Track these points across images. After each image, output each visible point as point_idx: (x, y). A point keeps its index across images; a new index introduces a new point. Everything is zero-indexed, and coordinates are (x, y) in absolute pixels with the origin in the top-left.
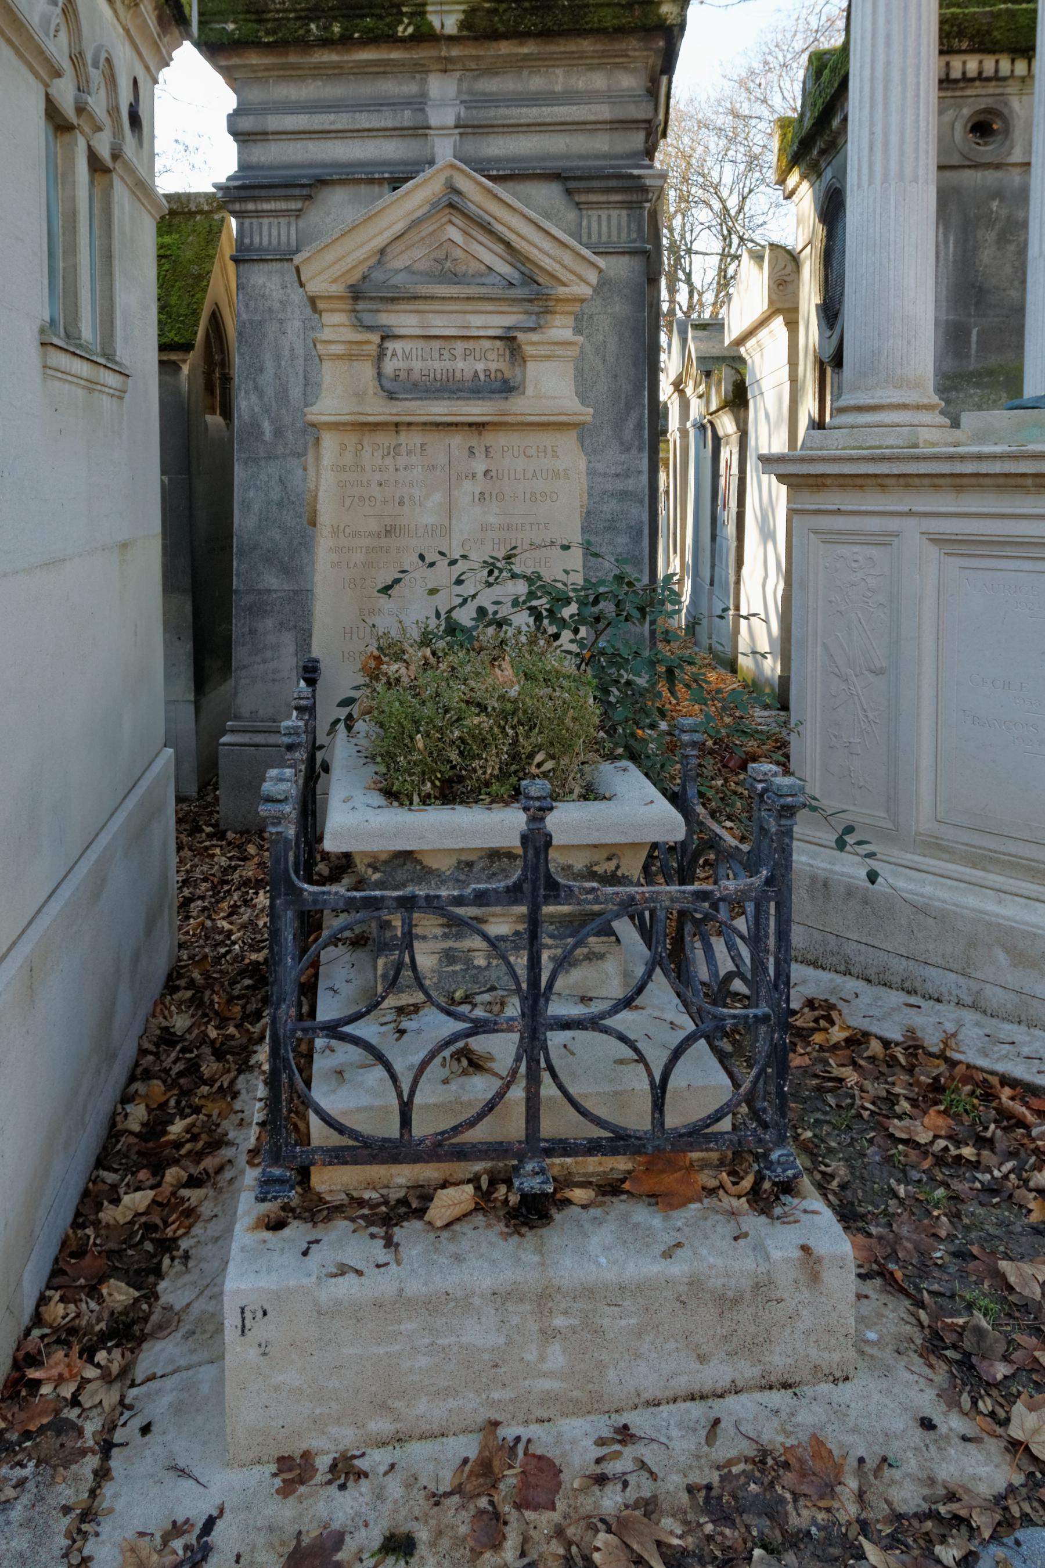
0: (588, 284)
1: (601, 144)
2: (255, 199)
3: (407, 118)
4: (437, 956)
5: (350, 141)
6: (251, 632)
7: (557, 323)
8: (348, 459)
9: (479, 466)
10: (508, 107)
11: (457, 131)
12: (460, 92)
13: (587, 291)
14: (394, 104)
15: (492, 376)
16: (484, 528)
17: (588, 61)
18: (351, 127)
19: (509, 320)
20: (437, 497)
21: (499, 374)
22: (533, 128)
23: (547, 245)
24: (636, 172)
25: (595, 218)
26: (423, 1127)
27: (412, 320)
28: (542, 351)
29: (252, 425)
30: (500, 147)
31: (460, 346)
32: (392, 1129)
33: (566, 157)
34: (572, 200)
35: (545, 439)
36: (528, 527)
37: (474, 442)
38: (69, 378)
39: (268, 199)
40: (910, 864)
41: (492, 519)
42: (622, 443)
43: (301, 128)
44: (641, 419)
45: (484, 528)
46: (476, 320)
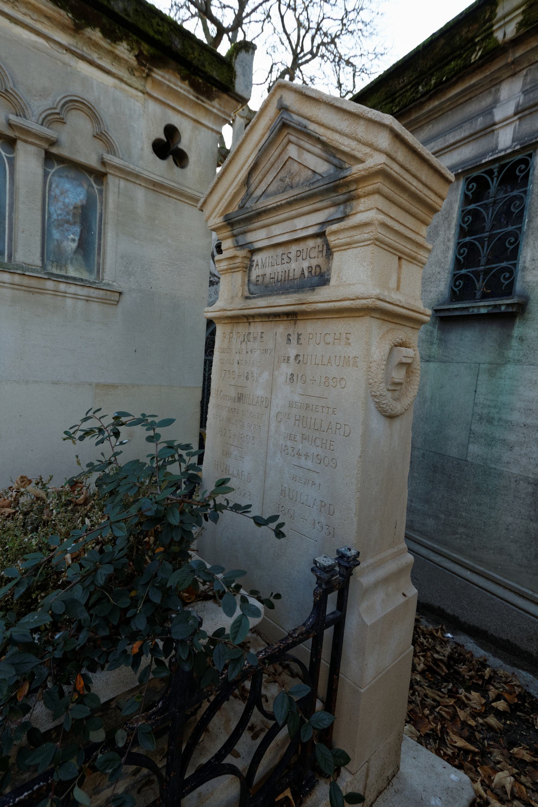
7: (361, 207)
9: (292, 352)
11: (516, 118)
16: (291, 405)
19: (321, 217)
20: (266, 375)
35: (340, 326)
36: (320, 409)
41: (297, 398)
45: (291, 405)
46: (300, 223)
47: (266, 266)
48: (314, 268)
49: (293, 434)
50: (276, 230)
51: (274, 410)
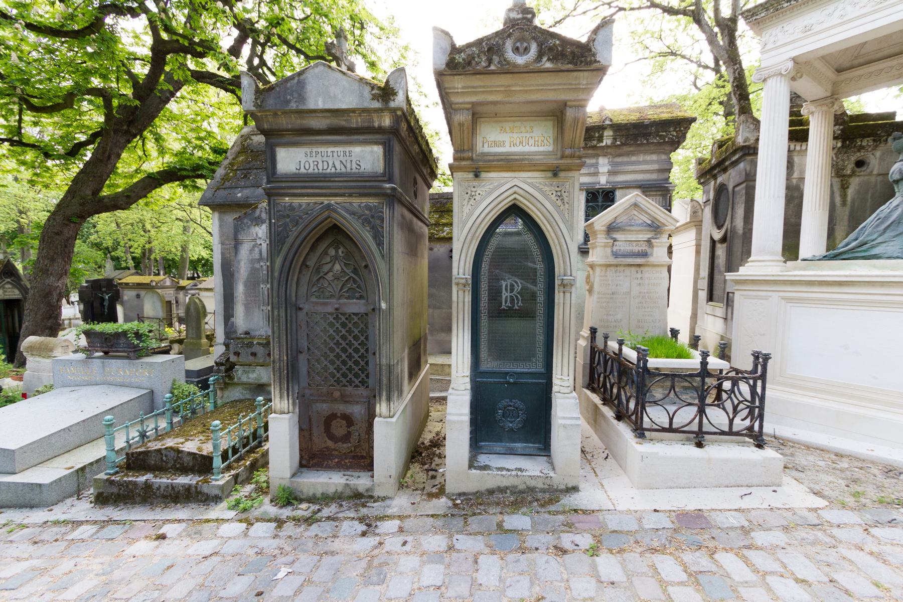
1: (654, 176)
3: (592, 170)
19: (649, 236)
26: (674, 426)
31: (634, 244)
46: (641, 236)
47: (621, 247)
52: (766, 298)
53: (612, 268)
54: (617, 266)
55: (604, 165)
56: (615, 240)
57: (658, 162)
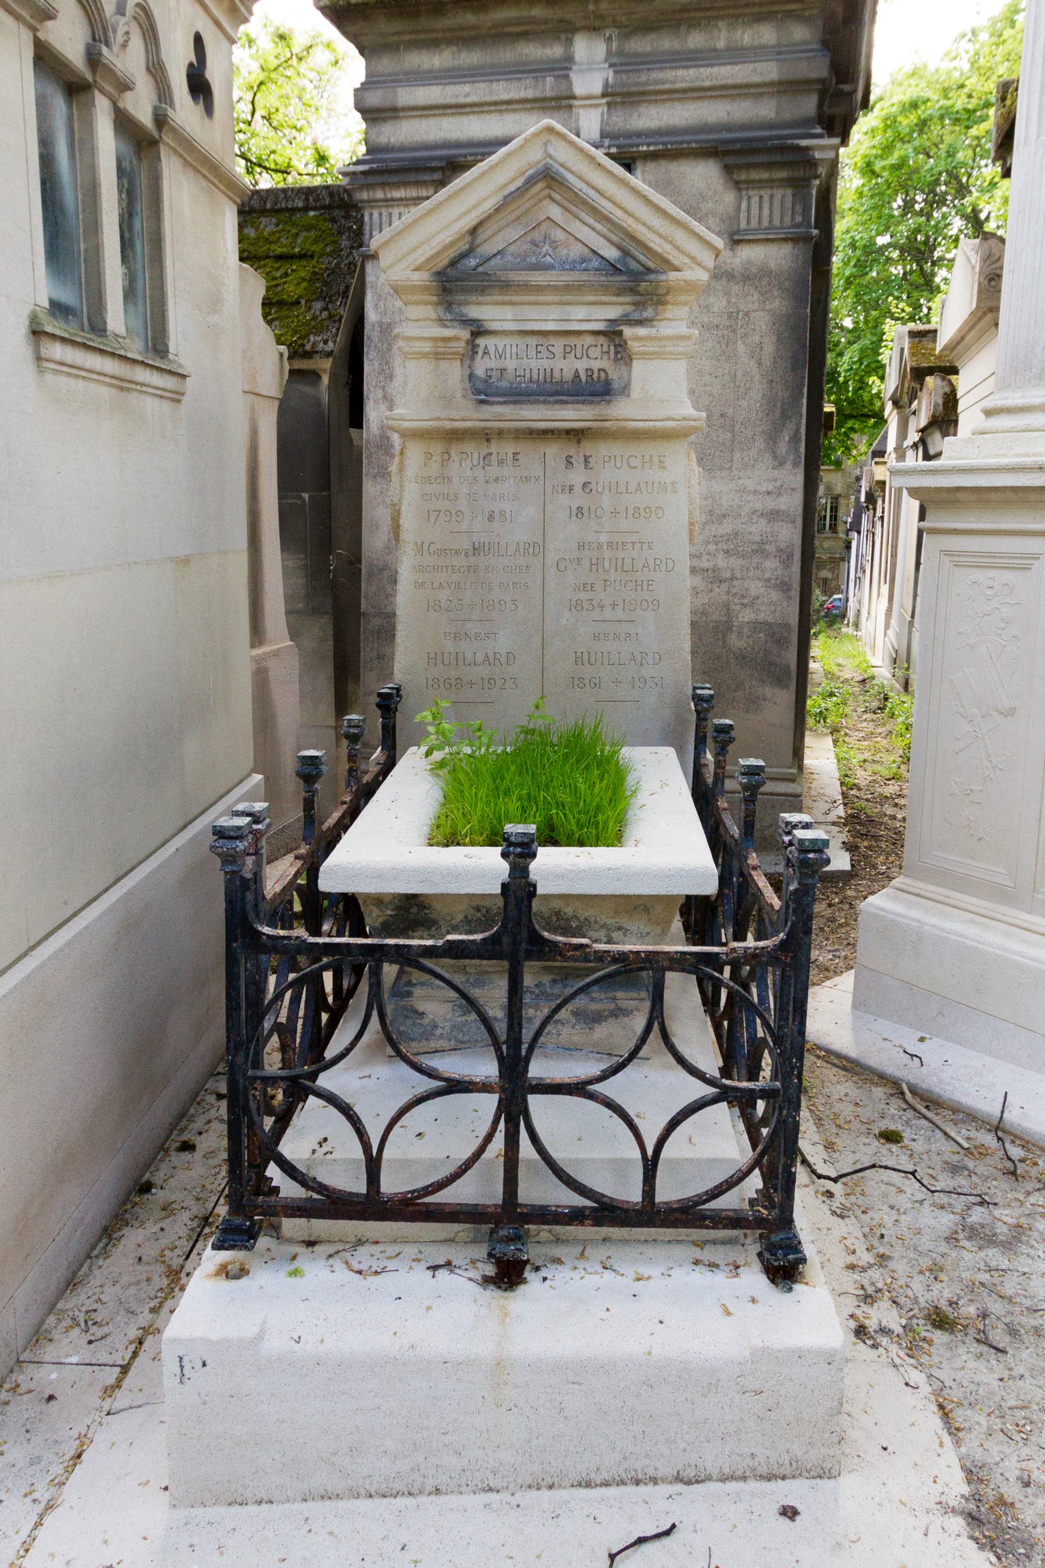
0: (704, 268)
1: (765, 110)
2: (383, 185)
3: (549, 86)
4: (451, 1005)
5: (488, 117)
6: (379, 657)
8: (434, 469)
10: (661, 69)
11: (604, 101)
12: (609, 53)
13: (704, 276)
14: (535, 71)
15: (595, 376)
17: (755, 10)
18: (488, 99)
19: (613, 312)
21: (603, 375)
22: (690, 95)
23: (657, 222)
24: (804, 143)
25: (755, 200)
26: (391, 1184)
27: (508, 312)
28: (651, 347)
29: (381, 437)
30: (651, 117)
31: (559, 344)
32: (360, 1187)
33: (728, 128)
34: (731, 178)
36: (630, 546)
37: (572, 451)
38: (83, 373)
39: (397, 185)
40: (1025, 925)
42: (775, 458)
43: (434, 102)
44: (797, 431)
46: (580, 312)
47: (506, 357)
48: (596, 371)
49: (590, 582)
50: (529, 312)
51: (552, 557)
52: (1022, 564)
53: (469, 447)
54: (486, 436)
55: (590, 67)
56: (478, 330)
57: (778, 52)
